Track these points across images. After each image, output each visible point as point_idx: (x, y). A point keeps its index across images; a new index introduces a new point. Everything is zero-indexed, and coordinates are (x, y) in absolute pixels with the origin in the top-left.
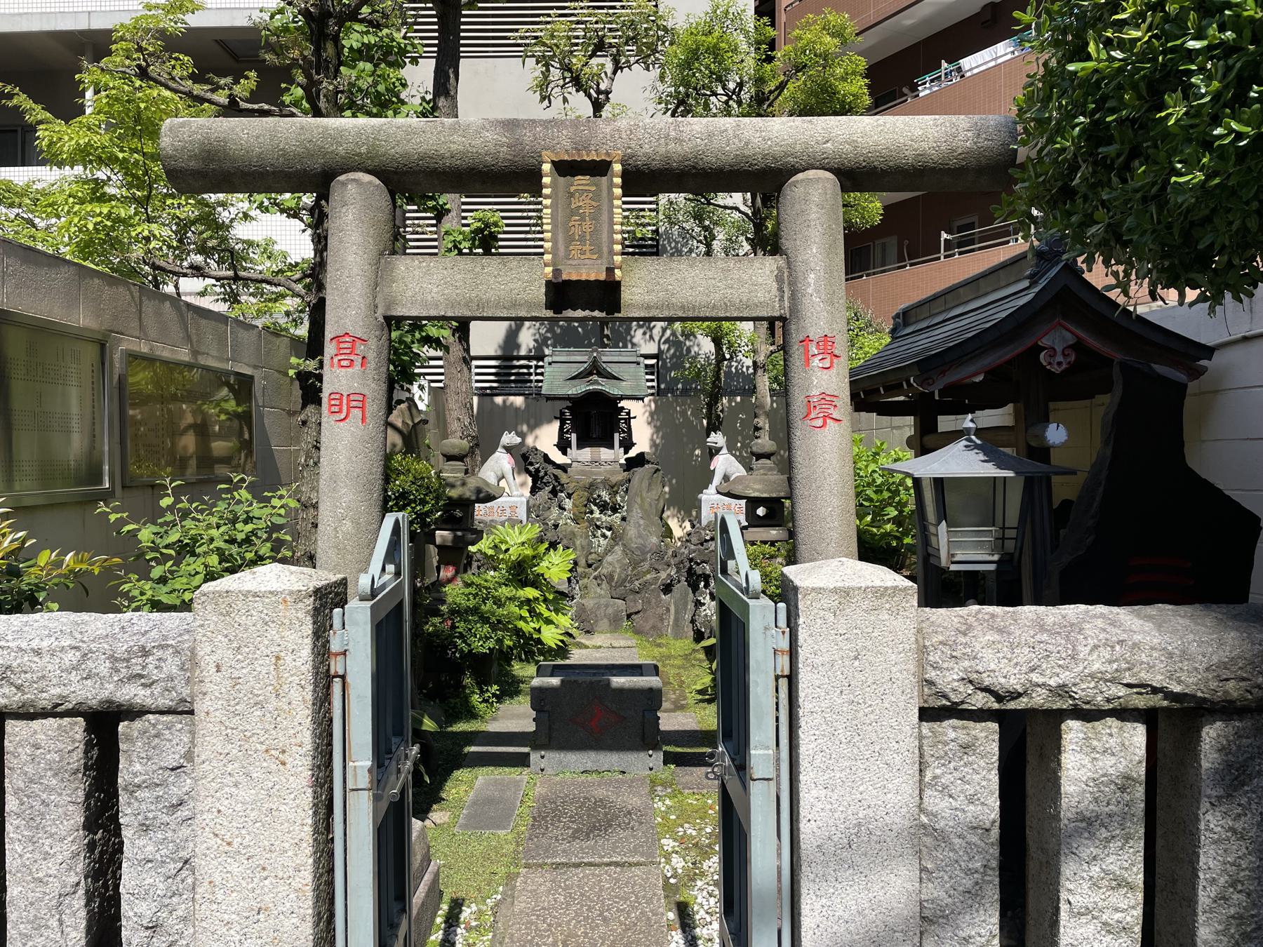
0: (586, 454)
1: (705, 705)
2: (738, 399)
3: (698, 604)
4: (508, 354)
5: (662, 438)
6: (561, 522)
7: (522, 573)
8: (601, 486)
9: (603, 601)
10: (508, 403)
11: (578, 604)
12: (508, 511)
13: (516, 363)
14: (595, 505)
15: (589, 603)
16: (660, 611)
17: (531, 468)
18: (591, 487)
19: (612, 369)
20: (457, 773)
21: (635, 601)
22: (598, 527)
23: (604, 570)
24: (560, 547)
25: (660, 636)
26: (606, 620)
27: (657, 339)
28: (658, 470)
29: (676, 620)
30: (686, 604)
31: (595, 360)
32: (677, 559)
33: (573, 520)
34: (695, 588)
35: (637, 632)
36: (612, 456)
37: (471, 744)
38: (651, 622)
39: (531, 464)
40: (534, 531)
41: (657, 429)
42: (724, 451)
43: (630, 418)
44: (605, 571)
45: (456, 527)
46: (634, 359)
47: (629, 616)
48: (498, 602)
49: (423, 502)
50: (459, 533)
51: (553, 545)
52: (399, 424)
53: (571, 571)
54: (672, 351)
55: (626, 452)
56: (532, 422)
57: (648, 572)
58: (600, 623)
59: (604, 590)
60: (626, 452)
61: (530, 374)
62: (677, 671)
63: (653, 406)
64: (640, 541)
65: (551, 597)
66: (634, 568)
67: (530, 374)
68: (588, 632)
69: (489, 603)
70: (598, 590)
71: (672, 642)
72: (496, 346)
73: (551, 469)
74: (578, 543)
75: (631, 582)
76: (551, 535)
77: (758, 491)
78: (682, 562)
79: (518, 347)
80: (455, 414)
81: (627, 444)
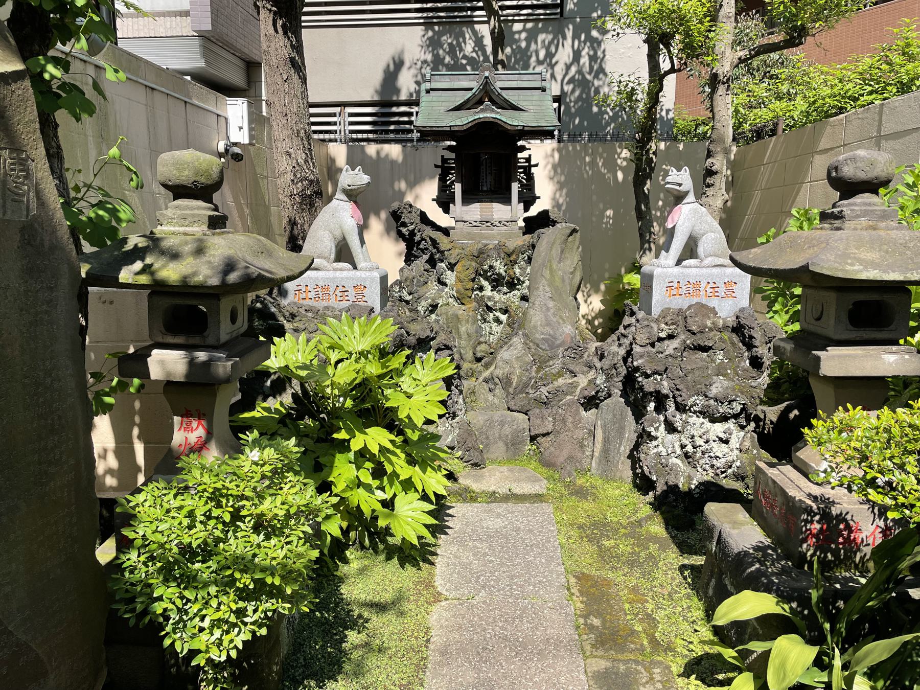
0: (475, 211)
4: (386, 98)
5: (567, 195)
6: (440, 302)
8: (494, 253)
10: (383, 155)
12: (352, 294)
13: (394, 109)
14: (486, 279)
15: (477, 418)
16: (580, 434)
17: (404, 230)
18: (480, 255)
19: (509, 96)
21: (543, 418)
22: (490, 309)
26: (501, 444)
27: (559, 78)
28: (574, 231)
29: (606, 452)
30: (621, 431)
31: (487, 83)
32: (606, 363)
33: (457, 299)
35: (547, 464)
36: (510, 213)
38: (565, 453)
39: (404, 225)
40: (383, 331)
41: (561, 186)
42: (691, 197)
43: (530, 166)
44: (499, 372)
46: (538, 84)
47: (533, 439)
50: (202, 356)
54: (577, 93)
55: (526, 209)
57: (560, 375)
59: (497, 398)
63: (557, 156)
64: (548, 330)
66: (539, 369)
68: (476, 465)
70: (490, 397)
73: (429, 232)
74: (463, 329)
75: (537, 388)
77: (874, 265)
78: (615, 367)
79: (398, 91)
80: (284, 146)
81: (528, 199)
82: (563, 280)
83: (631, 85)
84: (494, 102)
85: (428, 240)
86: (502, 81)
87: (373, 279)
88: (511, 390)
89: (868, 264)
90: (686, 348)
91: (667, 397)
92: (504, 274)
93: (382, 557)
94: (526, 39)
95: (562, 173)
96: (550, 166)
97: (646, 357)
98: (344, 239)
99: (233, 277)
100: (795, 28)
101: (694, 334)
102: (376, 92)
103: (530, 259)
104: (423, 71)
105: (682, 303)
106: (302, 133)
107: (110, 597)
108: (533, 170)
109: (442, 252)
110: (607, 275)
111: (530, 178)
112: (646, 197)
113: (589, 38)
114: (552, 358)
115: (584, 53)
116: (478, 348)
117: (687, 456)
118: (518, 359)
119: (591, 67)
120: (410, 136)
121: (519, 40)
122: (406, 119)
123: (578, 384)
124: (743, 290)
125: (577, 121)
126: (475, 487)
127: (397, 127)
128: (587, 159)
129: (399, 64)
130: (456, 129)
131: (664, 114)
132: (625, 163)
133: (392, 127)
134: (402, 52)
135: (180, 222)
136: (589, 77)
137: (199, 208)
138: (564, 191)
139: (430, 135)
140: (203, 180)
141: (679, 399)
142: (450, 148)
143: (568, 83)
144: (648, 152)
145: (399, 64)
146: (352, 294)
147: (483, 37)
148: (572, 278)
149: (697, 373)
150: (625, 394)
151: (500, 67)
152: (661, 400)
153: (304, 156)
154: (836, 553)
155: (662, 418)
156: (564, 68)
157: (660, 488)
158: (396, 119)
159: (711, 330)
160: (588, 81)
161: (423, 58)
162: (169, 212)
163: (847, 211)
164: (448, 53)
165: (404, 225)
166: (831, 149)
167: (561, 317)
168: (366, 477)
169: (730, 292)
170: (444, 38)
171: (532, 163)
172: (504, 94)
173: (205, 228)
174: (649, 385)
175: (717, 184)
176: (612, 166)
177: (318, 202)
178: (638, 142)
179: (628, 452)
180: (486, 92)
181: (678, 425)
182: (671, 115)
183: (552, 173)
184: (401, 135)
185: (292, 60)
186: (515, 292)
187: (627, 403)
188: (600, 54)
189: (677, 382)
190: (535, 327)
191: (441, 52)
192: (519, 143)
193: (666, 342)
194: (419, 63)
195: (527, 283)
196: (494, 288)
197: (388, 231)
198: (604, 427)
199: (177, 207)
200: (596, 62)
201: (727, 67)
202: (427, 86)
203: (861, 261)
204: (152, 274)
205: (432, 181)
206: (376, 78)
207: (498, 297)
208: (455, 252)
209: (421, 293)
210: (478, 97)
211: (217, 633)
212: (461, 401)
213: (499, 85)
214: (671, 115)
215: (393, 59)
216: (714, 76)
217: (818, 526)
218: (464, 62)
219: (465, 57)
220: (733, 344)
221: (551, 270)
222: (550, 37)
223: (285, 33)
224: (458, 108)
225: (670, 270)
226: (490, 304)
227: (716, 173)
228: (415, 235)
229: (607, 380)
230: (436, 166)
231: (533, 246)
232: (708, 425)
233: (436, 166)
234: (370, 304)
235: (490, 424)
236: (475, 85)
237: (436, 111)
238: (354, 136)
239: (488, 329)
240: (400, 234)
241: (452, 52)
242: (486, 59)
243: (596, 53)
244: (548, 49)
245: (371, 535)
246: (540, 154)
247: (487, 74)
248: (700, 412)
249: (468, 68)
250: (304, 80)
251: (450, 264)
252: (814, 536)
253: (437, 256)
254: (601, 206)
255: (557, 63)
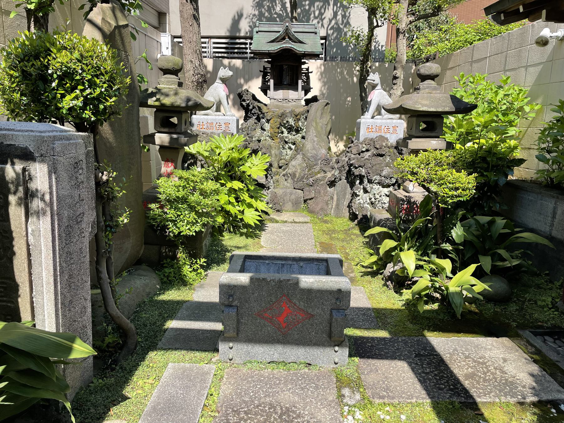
0: (280, 94)
1: (369, 278)
2: (377, 64)
3: (354, 195)
4: (233, 35)
5: (328, 89)
6: (262, 138)
7: (231, 170)
8: (289, 115)
9: (288, 191)
11: (272, 192)
12: (223, 126)
13: (238, 41)
14: (285, 128)
15: (279, 191)
16: (326, 198)
17: (244, 103)
18: (282, 116)
19: (300, 36)
20: (152, 355)
21: (310, 191)
22: (286, 142)
23: (290, 170)
24: (260, 153)
25: (326, 215)
26: (290, 203)
27: (326, 26)
28: (328, 104)
29: (338, 205)
30: (345, 194)
31: (287, 29)
32: (340, 165)
33: (271, 137)
34: (352, 185)
35: (311, 212)
36: (294, 97)
37: (172, 317)
38: (319, 207)
39: (244, 101)
40: (239, 140)
41: (325, 84)
42: (379, 87)
43: (309, 73)
44: (290, 171)
45: (172, 130)
47: (305, 201)
48: (204, 194)
49: (92, 85)
50: (175, 136)
51: (255, 152)
52: (99, 21)
53: (267, 170)
54: (335, 35)
55: (306, 94)
56: (247, 77)
57: (319, 173)
58: (286, 205)
60: (306, 94)
61: (246, 48)
62: (341, 244)
63: (323, 68)
64: (314, 152)
65: (252, 188)
66: (309, 170)
67: (246, 48)
68: (278, 211)
69: (197, 194)
70: (286, 183)
71: (334, 219)
72: (225, 30)
73: (256, 104)
74: (273, 152)
75: (307, 179)
76: (254, 146)
77: (426, 105)
78: (343, 166)
79: (239, 31)
81: (307, 90)
82: (322, 128)
83: (358, 32)
84: (290, 39)
85: (257, 107)
86: (295, 27)
87: (233, 120)
88: (296, 180)
89: (423, 105)
90: (374, 155)
91: (364, 176)
92: (294, 125)
93: (239, 235)
94: (308, 5)
95: (326, 77)
96: (319, 73)
97: (356, 160)
98: (220, 101)
99: (190, 103)
100: (435, 7)
101: (377, 149)
102: (228, 30)
103: (306, 118)
104: (253, 20)
105: (373, 135)
106: (198, 52)
107: (147, 217)
108: (310, 74)
109: (264, 114)
110: (347, 132)
111: (308, 78)
112: (365, 89)
113: (342, 6)
114: (315, 165)
115: (339, 13)
116: (280, 162)
117: (372, 203)
118: (299, 165)
119: (343, 21)
120: (246, 55)
121: (305, 5)
122: (243, 46)
123: (327, 176)
124: (401, 130)
125: (335, 50)
126: (277, 218)
127: (239, 51)
128: (339, 70)
129: (240, 16)
130: (272, 52)
131: (380, 47)
132: (358, 73)
133: (236, 51)
134: (242, 9)
135: (167, 83)
136: (341, 26)
137: (174, 78)
138: (327, 87)
139: (258, 55)
140: (176, 67)
141: (369, 177)
142: (268, 62)
143: (331, 29)
144: (366, 67)
145: (240, 16)
146: (223, 126)
147: (286, 3)
148: (326, 128)
149: (378, 166)
150: (347, 178)
151: (294, 20)
152: (361, 178)
153: (198, 62)
154: (413, 216)
155: (362, 187)
156: (328, 21)
157: (360, 217)
158: (238, 46)
159: (385, 147)
160: (341, 29)
161: (253, 13)
162: (163, 80)
163: (421, 87)
164: (267, 11)
165: (244, 101)
166: (454, 67)
167: (320, 145)
168: (233, 200)
169: (395, 131)
170: (265, 2)
171: (310, 71)
172: (296, 34)
173: (177, 86)
174: (356, 172)
175: (398, 83)
176: (351, 74)
177: (205, 86)
178: (361, 61)
179: (347, 204)
180: (287, 33)
181: (369, 189)
182: (384, 48)
183: (320, 77)
184: (241, 55)
185: (194, 15)
186: (299, 135)
187: (348, 182)
188: (347, 14)
189: (369, 169)
190: (308, 150)
191: (263, 10)
192: (303, 61)
193: (365, 153)
194: (251, 16)
195: (305, 130)
196: (289, 132)
197: (234, 105)
198: (337, 194)
199: (166, 78)
200: (345, 19)
201: (404, 26)
202: (256, 29)
203: (421, 104)
204: (160, 101)
205: (258, 79)
206: (228, 23)
207: (291, 137)
208: (270, 114)
209: (253, 134)
210: (283, 36)
211: (189, 226)
212: (272, 182)
213: (293, 30)
214: (384, 48)
215: (237, 13)
216: (398, 30)
217: (406, 206)
218: (275, 16)
219: (276, 13)
220: (394, 153)
221: (316, 123)
222: (321, 4)
223: (191, 2)
224: (272, 41)
225: (368, 120)
226: (286, 140)
227: (398, 78)
228: (249, 106)
229: (340, 173)
230: (261, 71)
231: (308, 111)
232: (381, 189)
233: (261, 71)
234: (231, 131)
235: (285, 194)
236: (281, 29)
237: (262, 42)
238: (217, 55)
239: (285, 153)
240: (242, 105)
241: (269, 10)
242: (287, 14)
243: (345, 14)
244: (320, 10)
245: (234, 227)
246: (313, 66)
247: (287, 24)
248: (378, 183)
249: (278, 19)
250: (199, 25)
251: (267, 119)
252: (405, 210)
253: (261, 116)
254: (345, 95)
255: (324, 18)
